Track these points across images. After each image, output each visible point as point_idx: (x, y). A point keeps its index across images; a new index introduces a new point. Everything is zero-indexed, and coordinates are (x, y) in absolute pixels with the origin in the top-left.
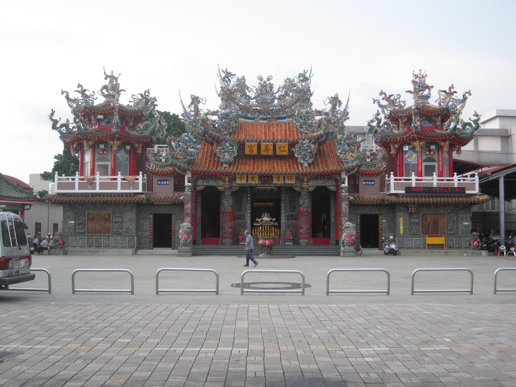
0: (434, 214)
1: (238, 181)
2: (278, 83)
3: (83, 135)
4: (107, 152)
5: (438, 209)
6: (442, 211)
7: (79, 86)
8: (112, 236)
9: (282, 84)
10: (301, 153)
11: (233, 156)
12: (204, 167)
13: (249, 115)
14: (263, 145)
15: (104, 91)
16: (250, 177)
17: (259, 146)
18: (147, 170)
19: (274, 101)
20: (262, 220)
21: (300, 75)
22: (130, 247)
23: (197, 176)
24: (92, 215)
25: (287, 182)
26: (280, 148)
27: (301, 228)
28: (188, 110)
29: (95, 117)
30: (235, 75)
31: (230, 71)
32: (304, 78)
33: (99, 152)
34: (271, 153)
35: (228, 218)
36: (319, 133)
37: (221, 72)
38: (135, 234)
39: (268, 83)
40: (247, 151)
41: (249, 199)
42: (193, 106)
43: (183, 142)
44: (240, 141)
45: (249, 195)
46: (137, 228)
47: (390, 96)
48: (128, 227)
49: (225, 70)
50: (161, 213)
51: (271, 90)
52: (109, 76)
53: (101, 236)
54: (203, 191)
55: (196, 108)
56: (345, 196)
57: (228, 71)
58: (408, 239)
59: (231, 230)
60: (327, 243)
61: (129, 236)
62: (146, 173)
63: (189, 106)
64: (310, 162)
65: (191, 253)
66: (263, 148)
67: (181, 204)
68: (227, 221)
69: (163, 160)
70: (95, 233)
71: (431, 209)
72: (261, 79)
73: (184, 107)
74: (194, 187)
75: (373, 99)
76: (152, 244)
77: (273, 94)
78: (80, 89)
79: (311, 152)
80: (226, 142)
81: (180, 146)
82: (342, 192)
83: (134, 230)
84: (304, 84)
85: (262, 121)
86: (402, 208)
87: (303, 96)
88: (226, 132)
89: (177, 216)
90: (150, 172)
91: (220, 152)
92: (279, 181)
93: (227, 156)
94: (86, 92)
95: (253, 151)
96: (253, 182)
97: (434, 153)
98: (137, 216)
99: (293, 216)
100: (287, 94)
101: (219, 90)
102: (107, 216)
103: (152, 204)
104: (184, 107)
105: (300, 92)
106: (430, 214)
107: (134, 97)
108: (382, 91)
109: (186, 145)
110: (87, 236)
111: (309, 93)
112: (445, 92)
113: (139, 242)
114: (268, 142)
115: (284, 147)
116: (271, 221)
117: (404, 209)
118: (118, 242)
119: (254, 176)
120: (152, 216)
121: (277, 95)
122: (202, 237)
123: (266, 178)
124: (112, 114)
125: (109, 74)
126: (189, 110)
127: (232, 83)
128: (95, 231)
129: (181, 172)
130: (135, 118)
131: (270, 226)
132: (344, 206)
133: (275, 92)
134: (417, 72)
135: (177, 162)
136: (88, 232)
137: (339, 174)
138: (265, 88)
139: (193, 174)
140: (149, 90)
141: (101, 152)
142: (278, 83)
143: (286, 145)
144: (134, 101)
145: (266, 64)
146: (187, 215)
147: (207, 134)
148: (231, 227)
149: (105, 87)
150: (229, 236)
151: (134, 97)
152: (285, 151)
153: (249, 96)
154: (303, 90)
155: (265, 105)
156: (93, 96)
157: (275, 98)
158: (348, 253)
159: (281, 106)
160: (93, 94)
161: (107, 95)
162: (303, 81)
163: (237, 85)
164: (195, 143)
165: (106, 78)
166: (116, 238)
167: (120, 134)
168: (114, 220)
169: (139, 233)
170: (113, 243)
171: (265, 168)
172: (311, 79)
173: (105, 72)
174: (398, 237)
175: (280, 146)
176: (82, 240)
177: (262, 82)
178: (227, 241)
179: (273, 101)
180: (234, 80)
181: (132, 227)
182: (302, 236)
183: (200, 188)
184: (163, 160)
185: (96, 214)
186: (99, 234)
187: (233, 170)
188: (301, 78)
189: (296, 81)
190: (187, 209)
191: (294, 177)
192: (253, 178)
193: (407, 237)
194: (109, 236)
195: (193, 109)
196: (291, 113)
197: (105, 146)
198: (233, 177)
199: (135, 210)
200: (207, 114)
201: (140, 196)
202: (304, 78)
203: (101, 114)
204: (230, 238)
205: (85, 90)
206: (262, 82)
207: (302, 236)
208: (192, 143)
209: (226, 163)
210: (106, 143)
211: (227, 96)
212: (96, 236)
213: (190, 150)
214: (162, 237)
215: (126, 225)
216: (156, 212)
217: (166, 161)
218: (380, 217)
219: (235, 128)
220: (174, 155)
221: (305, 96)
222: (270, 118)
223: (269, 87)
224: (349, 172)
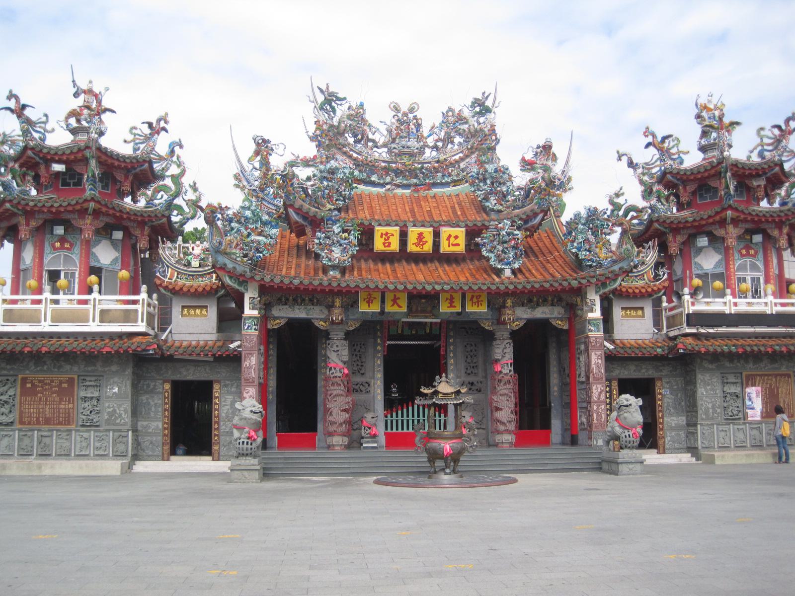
0: (770, 375)
1: (363, 308)
2: (430, 118)
3: (15, 202)
4: (72, 245)
5: (776, 365)
6: (784, 370)
7: (11, 96)
8: (77, 431)
9: (438, 120)
10: (495, 248)
11: (350, 252)
12: (293, 272)
13: (374, 178)
14: (413, 233)
15: (73, 121)
16: (389, 297)
17: (404, 235)
18: (158, 282)
19: (424, 153)
20: (436, 393)
21: (477, 102)
22: (116, 456)
23: (272, 295)
24: (32, 382)
25: (470, 309)
26: (448, 239)
27: (498, 409)
28: (248, 167)
29: (48, 167)
30: (345, 99)
31: (335, 91)
32: (482, 107)
33: (53, 246)
34: (428, 248)
35: (338, 390)
36: (527, 208)
37: (317, 92)
38: (128, 427)
39: (411, 116)
40: (379, 245)
41: (379, 348)
42: (259, 158)
43: (239, 222)
44: (362, 224)
45: (379, 341)
46: (135, 413)
47: (664, 139)
48: (114, 411)
49: (324, 88)
50: (190, 378)
51: (417, 131)
52: (85, 92)
53: (52, 430)
54: (278, 331)
55: (265, 163)
56: (596, 338)
57: (331, 90)
58: (721, 428)
59: (346, 416)
60: (546, 442)
61: (114, 431)
62: (158, 292)
63: (250, 160)
64: (516, 266)
65: (262, 471)
66: (412, 238)
67: (234, 360)
68: (337, 395)
69: (195, 263)
70: (38, 423)
71: (762, 365)
72: (396, 109)
73: (239, 161)
74: (264, 318)
75: (618, 152)
76: (167, 448)
77: (420, 138)
78: (12, 104)
79: (515, 247)
80: (335, 223)
81: (232, 229)
82: (590, 331)
83: (126, 418)
84: (482, 120)
85: (399, 191)
86: (706, 364)
87: (481, 143)
88: (329, 206)
89: (226, 386)
90: (166, 288)
91: (320, 244)
92: (451, 306)
93: (337, 253)
94: (27, 112)
95: (390, 243)
96: (395, 309)
97: (756, 252)
98: (135, 386)
99: (472, 384)
100: (449, 139)
101: (312, 128)
102: (65, 385)
103: (170, 359)
104: (239, 161)
105: (476, 134)
106: (761, 375)
107: (134, 131)
108: (647, 128)
109: (246, 229)
110: (20, 430)
111: (494, 138)
112: (779, 127)
113: (137, 443)
114: (423, 226)
115: (456, 237)
116: (458, 393)
117: (710, 366)
118: (89, 444)
119: (398, 295)
120: (167, 386)
121: (430, 141)
122: (278, 431)
123: (425, 300)
124: (85, 161)
125: (84, 87)
126: (251, 167)
127: (339, 113)
128: (38, 419)
129: (236, 286)
130: (136, 176)
131: (424, 406)
132: (596, 360)
133: (425, 134)
134: (702, 101)
135: (227, 261)
136: (22, 422)
137: (580, 292)
138: (406, 124)
139: (263, 290)
140: (167, 114)
141: (58, 245)
142: (430, 118)
143: (461, 232)
144: (133, 141)
145: (407, 80)
146: (249, 382)
147: (292, 206)
148: (345, 410)
149: (73, 114)
150: (340, 430)
151: (134, 131)
152: (458, 245)
153: (373, 141)
154: (481, 130)
155: (405, 159)
156: (45, 123)
157: (426, 146)
158: (631, 466)
159: (438, 162)
160: (44, 119)
161: (75, 128)
162: (480, 114)
163: (350, 117)
164: (265, 224)
165: (76, 95)
166: (85, 435)
167: (99, 202)
168: (83, 394)
169: (140, 424)
170: (78, 446)
171: (420, 277)
172: (494, 109)
173: (73, 81)
174: (702, 425)
175: (450, 236)
176: (6, 439)
177: (400, 115)
178: (337, 440)
179: (421, 152)
180: (341, 110)
181: (124, 409)
182: (501, 428)
183: (273, 325)
184: (195, 263)
185: (40, 381)
186: (46, 427)
187: (351, 280)
188: (478, 109)
189: (467, 113)
190: (250, 367)
191: (484, 298)
192: (395, 301)
193: (718, 424)
194: (70, 430)
195: (257, 165)
196: (458, 175)
197: (65, 230)
198: (350, 298)
199: (129, 371)
200: (292, 164)
201: (138, 339)
202: (482, 107)
203: (59, 162)
204: (343, 435)
205: (24, 107)
206: (400, 115)
207: (501, 428)
208: (259, 224)
209: (334, 267)
210: (68, 225)
211: (329, 138)
212: (39, 430)
213: (254, 237)
214: (191, 431)
215: (107, 406)
216: (177, 377)
217: (200, 266)
218: (658, 384)
219: (349, 198)
220: (220, 243)
221: (483, 142)
222: (416, 185)
223: (414, 124)
224: (604, 285)
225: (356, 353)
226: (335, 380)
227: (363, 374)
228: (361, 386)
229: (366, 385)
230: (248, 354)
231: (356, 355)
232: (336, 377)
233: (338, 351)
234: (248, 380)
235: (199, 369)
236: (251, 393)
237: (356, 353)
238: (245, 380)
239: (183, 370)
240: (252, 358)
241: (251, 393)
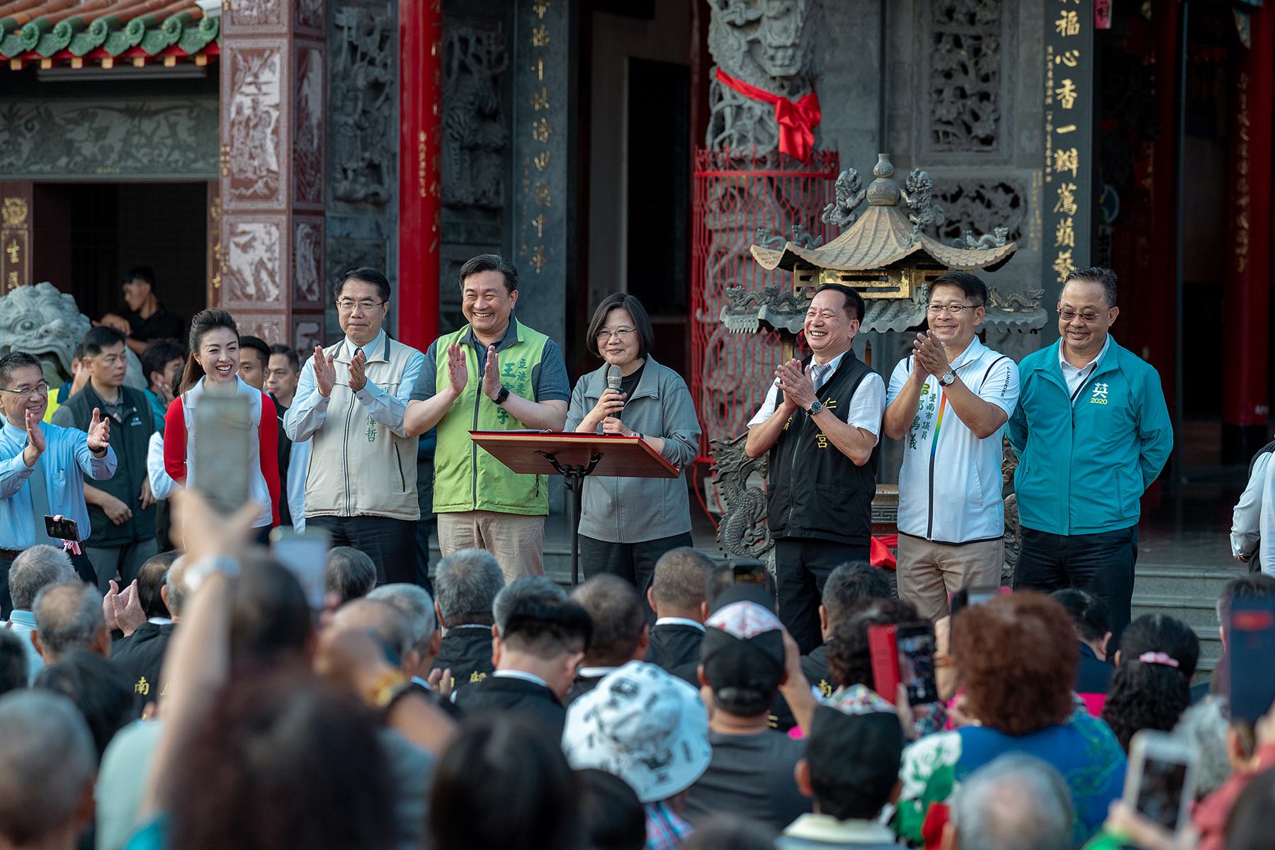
216: (59, 169)
225: (952, 28)
226: (742, 177)
227: (987, 141)
228: (978, 209)
229: (1000, 199)
230: (249, 54)
231: (958, 43)
232: (740, 162)
233: (754, 23)
234: (249, 183)
235: (147, 126)
236: (259, 252)
237: (952, 28)
238: (236, 183)
239: (79, 134)
240: (265, 76)
241: (259, 252)
